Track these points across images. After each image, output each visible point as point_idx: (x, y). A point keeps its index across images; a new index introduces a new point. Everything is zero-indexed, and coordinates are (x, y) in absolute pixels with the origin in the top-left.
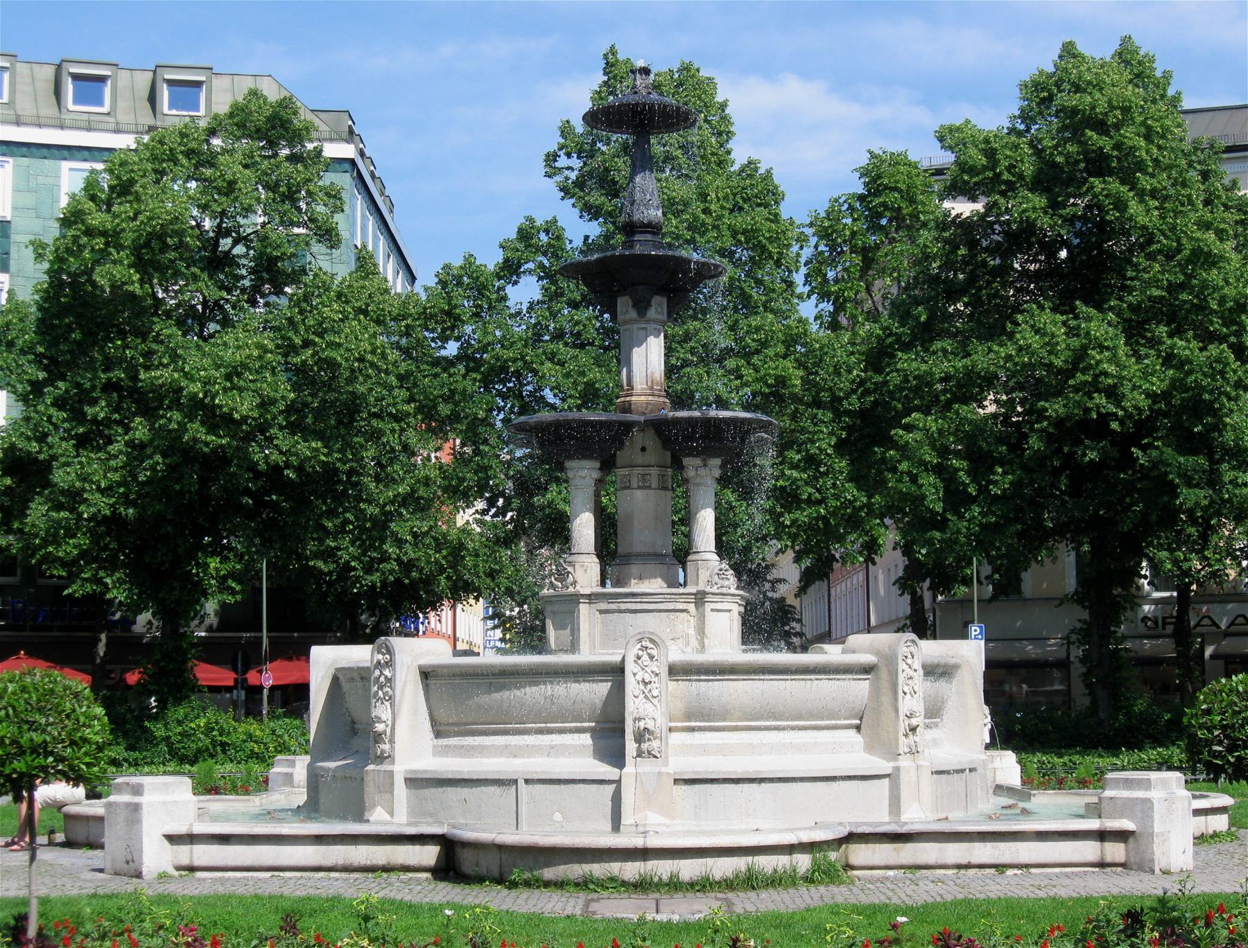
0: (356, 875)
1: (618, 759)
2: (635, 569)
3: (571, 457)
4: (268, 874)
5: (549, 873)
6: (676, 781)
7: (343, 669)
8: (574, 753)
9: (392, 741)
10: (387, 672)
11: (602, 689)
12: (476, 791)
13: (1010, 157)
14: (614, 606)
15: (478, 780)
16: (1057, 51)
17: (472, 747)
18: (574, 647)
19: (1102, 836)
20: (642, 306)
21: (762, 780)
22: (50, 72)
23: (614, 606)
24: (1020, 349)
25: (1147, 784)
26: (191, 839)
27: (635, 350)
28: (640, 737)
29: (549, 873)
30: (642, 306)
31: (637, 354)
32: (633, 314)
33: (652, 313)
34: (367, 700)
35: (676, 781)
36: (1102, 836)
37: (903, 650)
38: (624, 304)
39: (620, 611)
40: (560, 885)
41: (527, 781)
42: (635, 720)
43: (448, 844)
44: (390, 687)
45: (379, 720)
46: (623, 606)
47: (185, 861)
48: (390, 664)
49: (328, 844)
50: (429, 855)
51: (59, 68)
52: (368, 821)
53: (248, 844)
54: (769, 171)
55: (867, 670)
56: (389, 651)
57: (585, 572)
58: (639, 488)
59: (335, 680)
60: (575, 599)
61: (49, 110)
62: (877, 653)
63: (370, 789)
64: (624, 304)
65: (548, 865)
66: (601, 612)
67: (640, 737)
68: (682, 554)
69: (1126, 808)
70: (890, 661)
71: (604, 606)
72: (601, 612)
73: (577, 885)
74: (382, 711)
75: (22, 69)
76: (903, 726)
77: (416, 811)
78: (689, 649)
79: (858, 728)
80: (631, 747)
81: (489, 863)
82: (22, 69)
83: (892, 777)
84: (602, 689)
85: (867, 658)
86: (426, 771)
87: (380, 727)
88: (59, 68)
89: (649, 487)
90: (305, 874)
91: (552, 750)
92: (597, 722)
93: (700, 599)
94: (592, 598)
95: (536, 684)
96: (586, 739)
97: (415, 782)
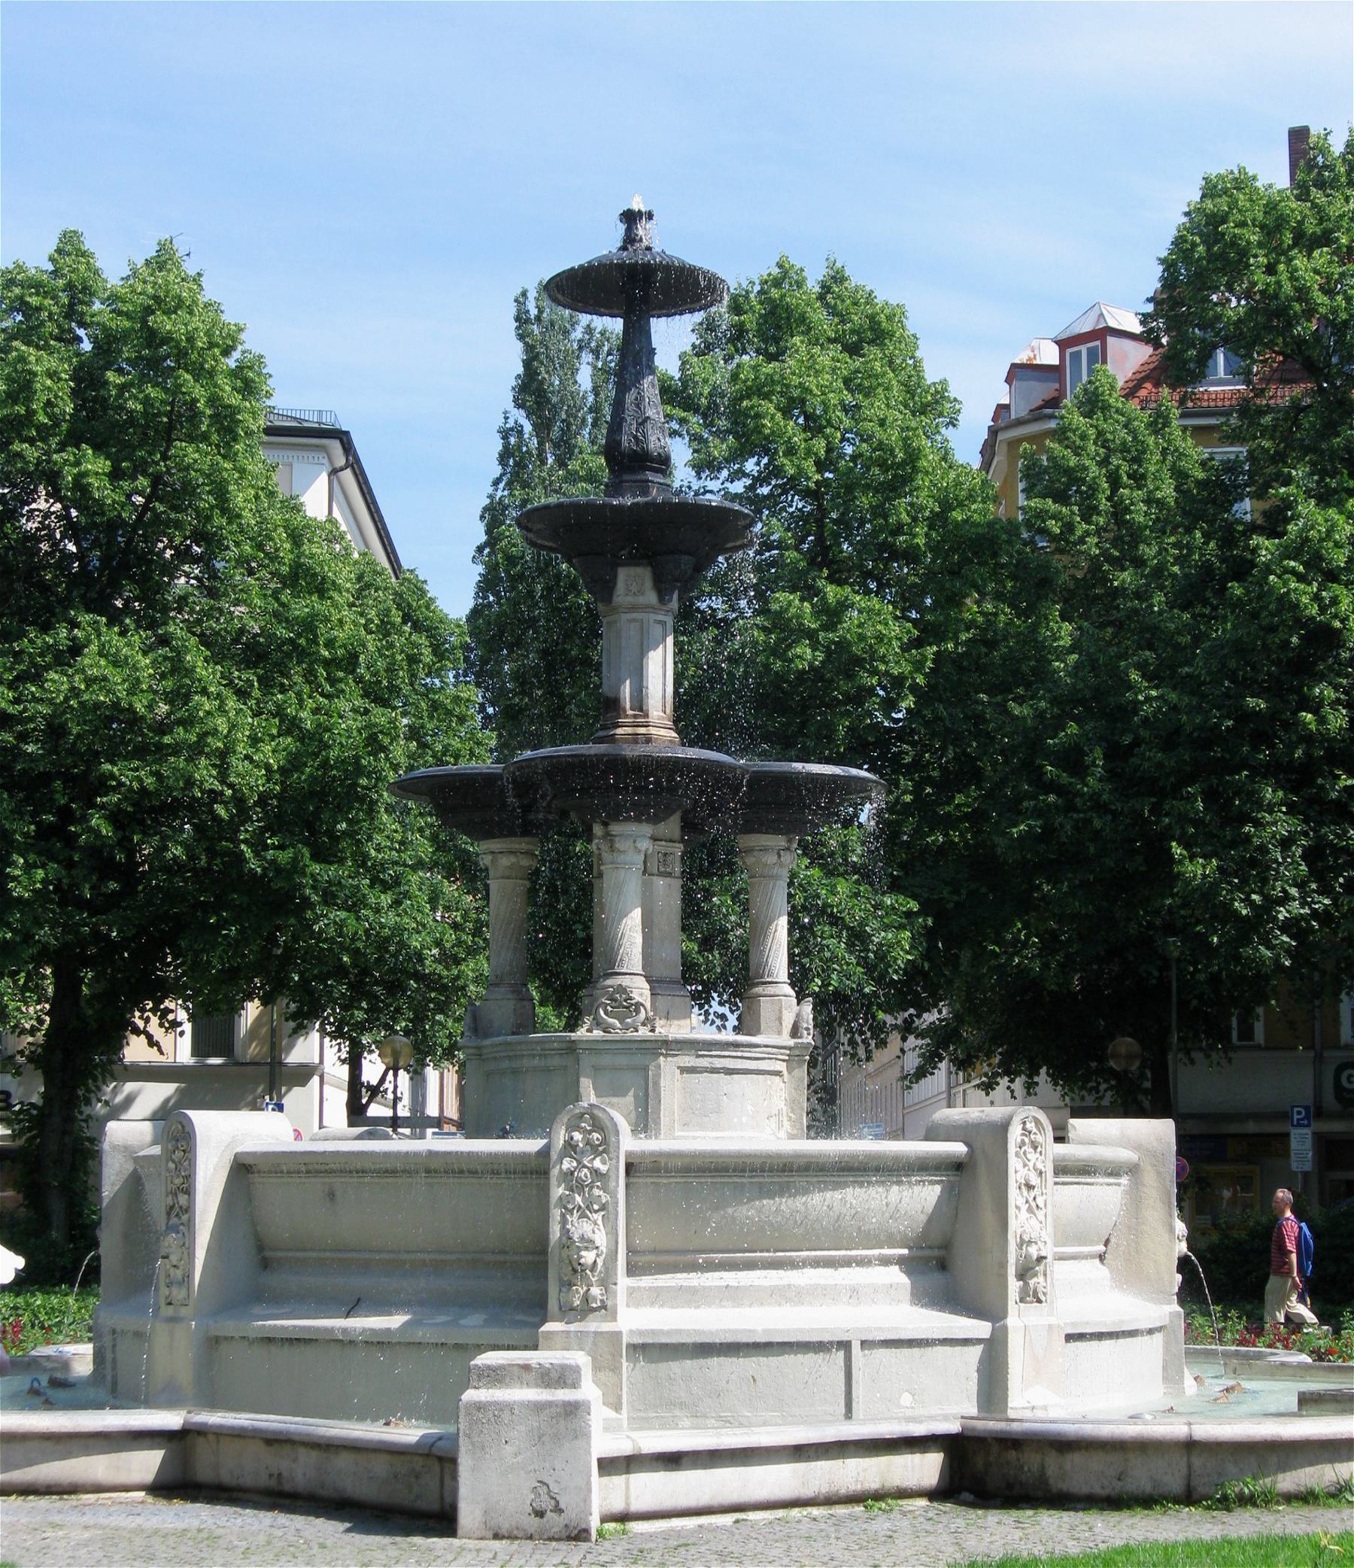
0: (841, 1510)
4: (727, 1519)
5: (1288, 1481)
6: (1070, 1338)
8: (876, 1298)
12: (774, 1361)
13: (49, 389)
14: (704, 1062)
15: (747, 1345)
16: (51, 247)
17: (693, 1291)
23: (704, 1062)
24: (90, 681)
27: (651, 654)
29: (1288, 1481)
35: (1070, 1338)
39: (714, 1071)
40: (1306, 1497)
41: (864, 1344)
42: (1020, 1246)
44: (605, 1189)
46: (719, 1063)
47: (618, 1506)
49: (808, 1459)
50: (927, 1468)
53: (705, 1466)
58: (660, 874)
62: (1137, 1147)
65: (1284, 1468)
66: (684, 1070)
71: (689, 1061)
72: (684, 1070)
73: (1333, 1496)
78: (782, 1134)
79: (1101, 1257)
86: (679, 1332)
89: (669, 875)
90: (780, 1513)
91: (733, 1295)
92: (910, 1248)
95: (837, 1186)
96: (896, 1276)
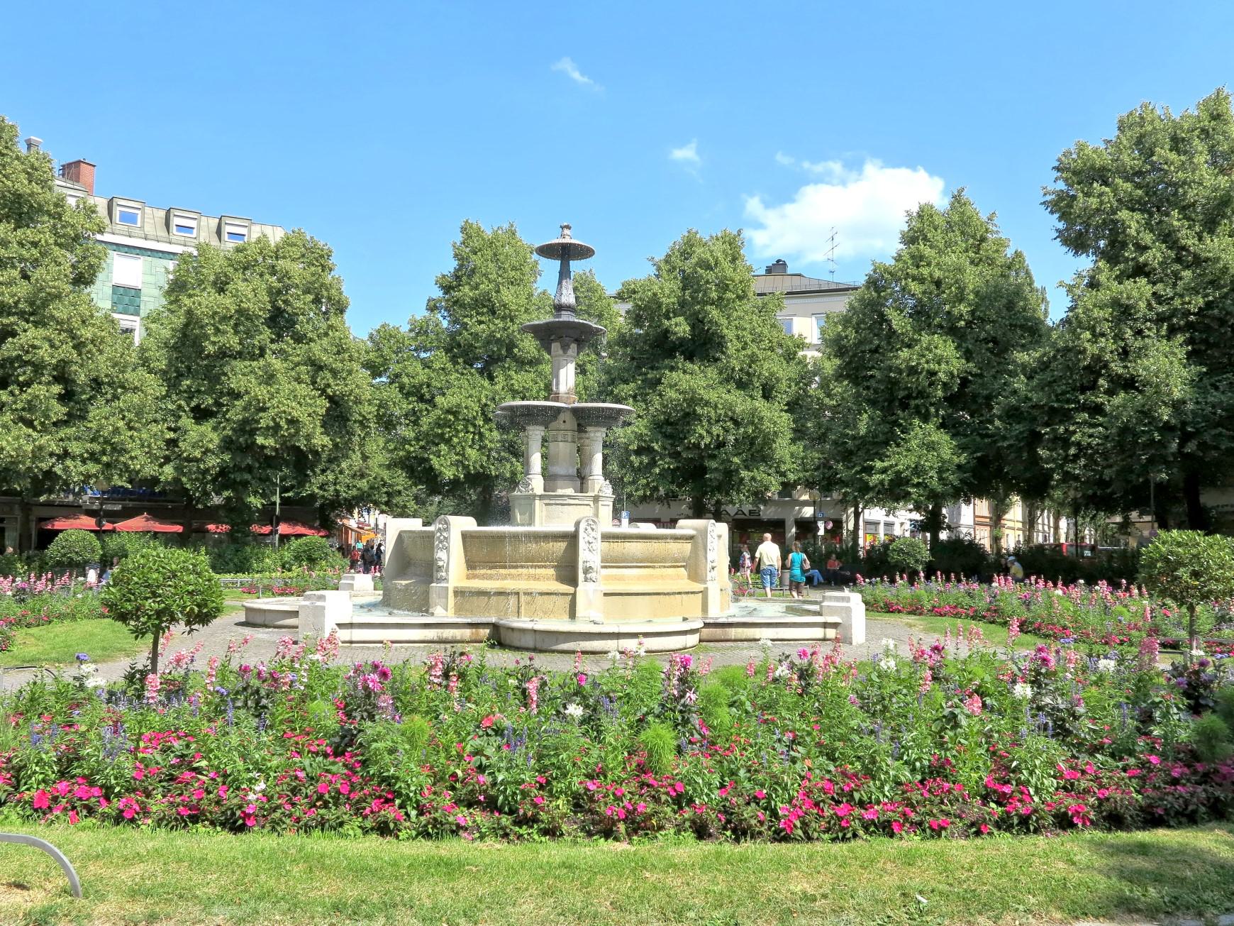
1: (573, 581)
2: (559, 483)
3: (529, 424)
6: (605, 594)
7: (405, 532)
8: (545, 580)
9: (447, 571)
10: (445, 534)
11: (561, 546)
18: (531, 522)
19: (825, 625)
20: (565, 348)
21: (668, 594)
22: (162, 214)
25: (322, 598)
26: (351, 626)
28: (586, 571)
30: (565, 348)
31: (562, 372)
32: (561, 352)
33: (570, 352)
34: (431, 548)
35: (605, 594)
36: (825, 625)
37: (710, 529)
38: (556, 347)
43: (495, 627)
45: (440, 559)
48: (447, 530)
50: (485, 632)
51: (168, 212)
52: (432, 614)
54: (1018, 254)
55: (691, 538)
56: (447, 523)
57: (537, 483)
59: (400, 536)
60: (535, 496)
61: (163, 233)
63: (433, 597)
64: (556, 347)
67: (586, 571)
68: (581, 479)
69: (833, 611)
70: (704, 533)
74: (441, 555)
75: (148, 210)
76: (709, 566)
77: (459, 610)
80: (581, 576)
81: (528, 641)
82: (148, 210)
83: (704, 593)
84: (561, 546)
85: (692, 532)
87: (440, 563)
88: (168, 212)
93: (596, 499)
94: (541, 497)
96: (552, 572)
97: (459, 593)
